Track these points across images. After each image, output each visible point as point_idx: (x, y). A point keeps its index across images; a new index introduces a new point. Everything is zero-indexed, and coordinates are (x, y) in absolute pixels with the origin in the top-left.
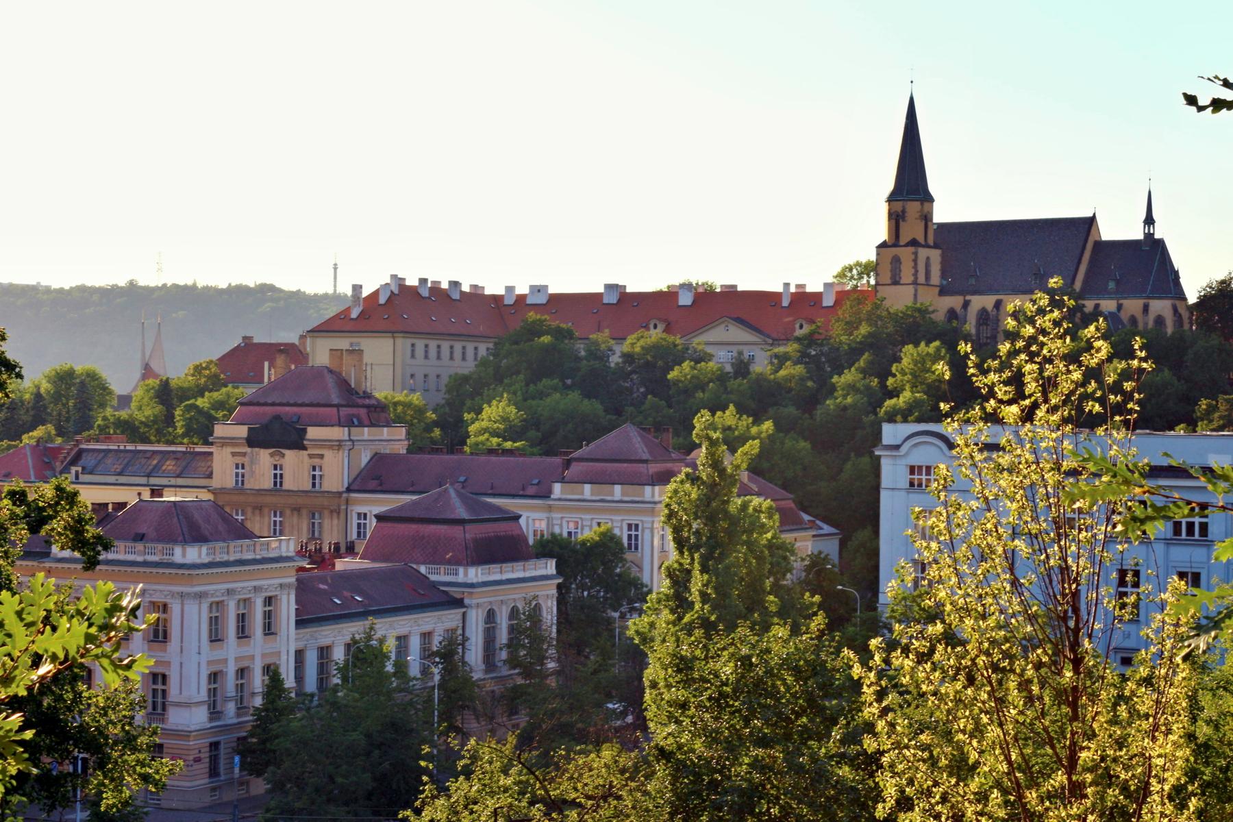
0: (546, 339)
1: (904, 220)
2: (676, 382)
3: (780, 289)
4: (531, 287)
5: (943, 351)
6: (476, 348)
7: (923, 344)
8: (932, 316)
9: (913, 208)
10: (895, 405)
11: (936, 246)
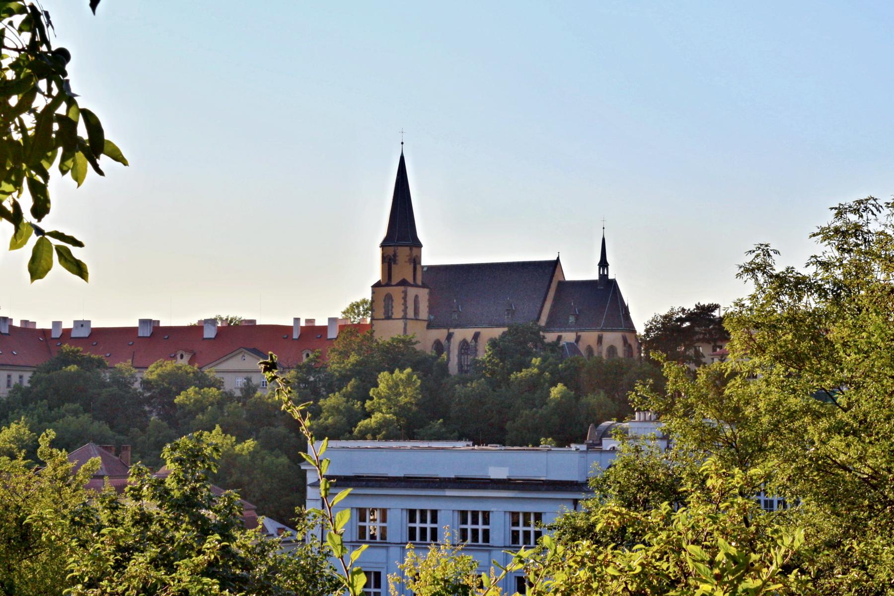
0: (73, 368)
1: (395, 263)
2: (182, 406)
3: (290, 323)
4: (76, 322)
5: (415, 377)
6: (9, 376)
7: (397, 371)
8: (415, 346)
9: (403, 252)
10: (367, 424)
11: (424, 286)
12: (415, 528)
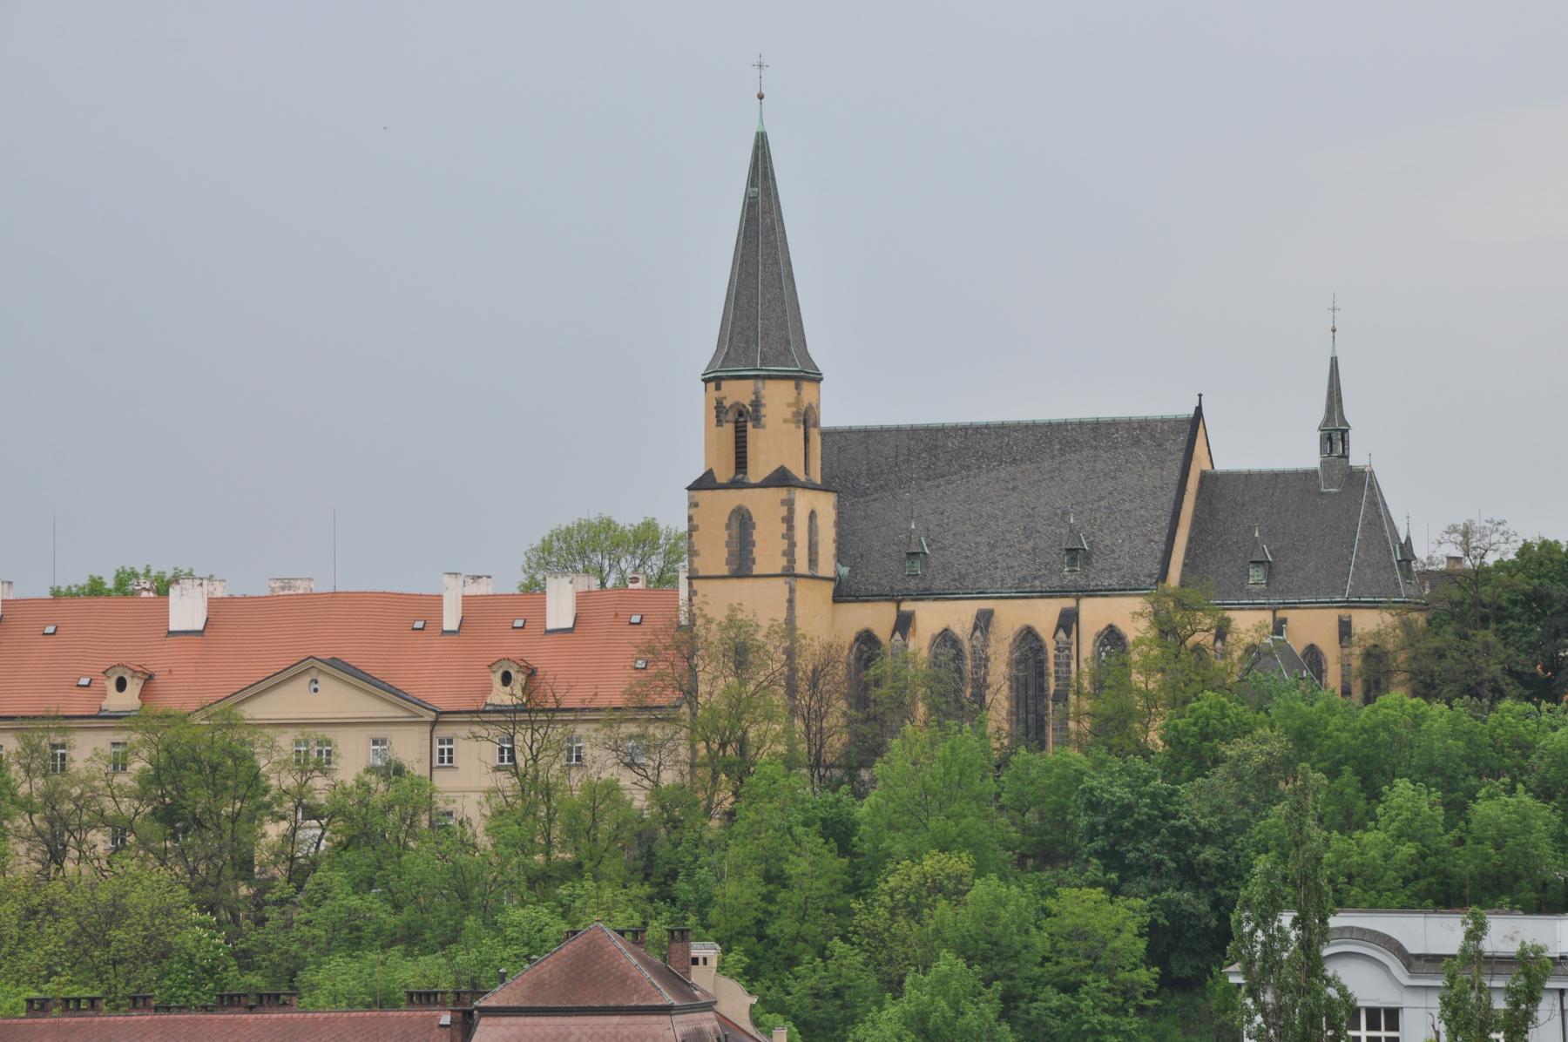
9: (778, 398)
11: (825, 488)
12: (1368, 1028)
